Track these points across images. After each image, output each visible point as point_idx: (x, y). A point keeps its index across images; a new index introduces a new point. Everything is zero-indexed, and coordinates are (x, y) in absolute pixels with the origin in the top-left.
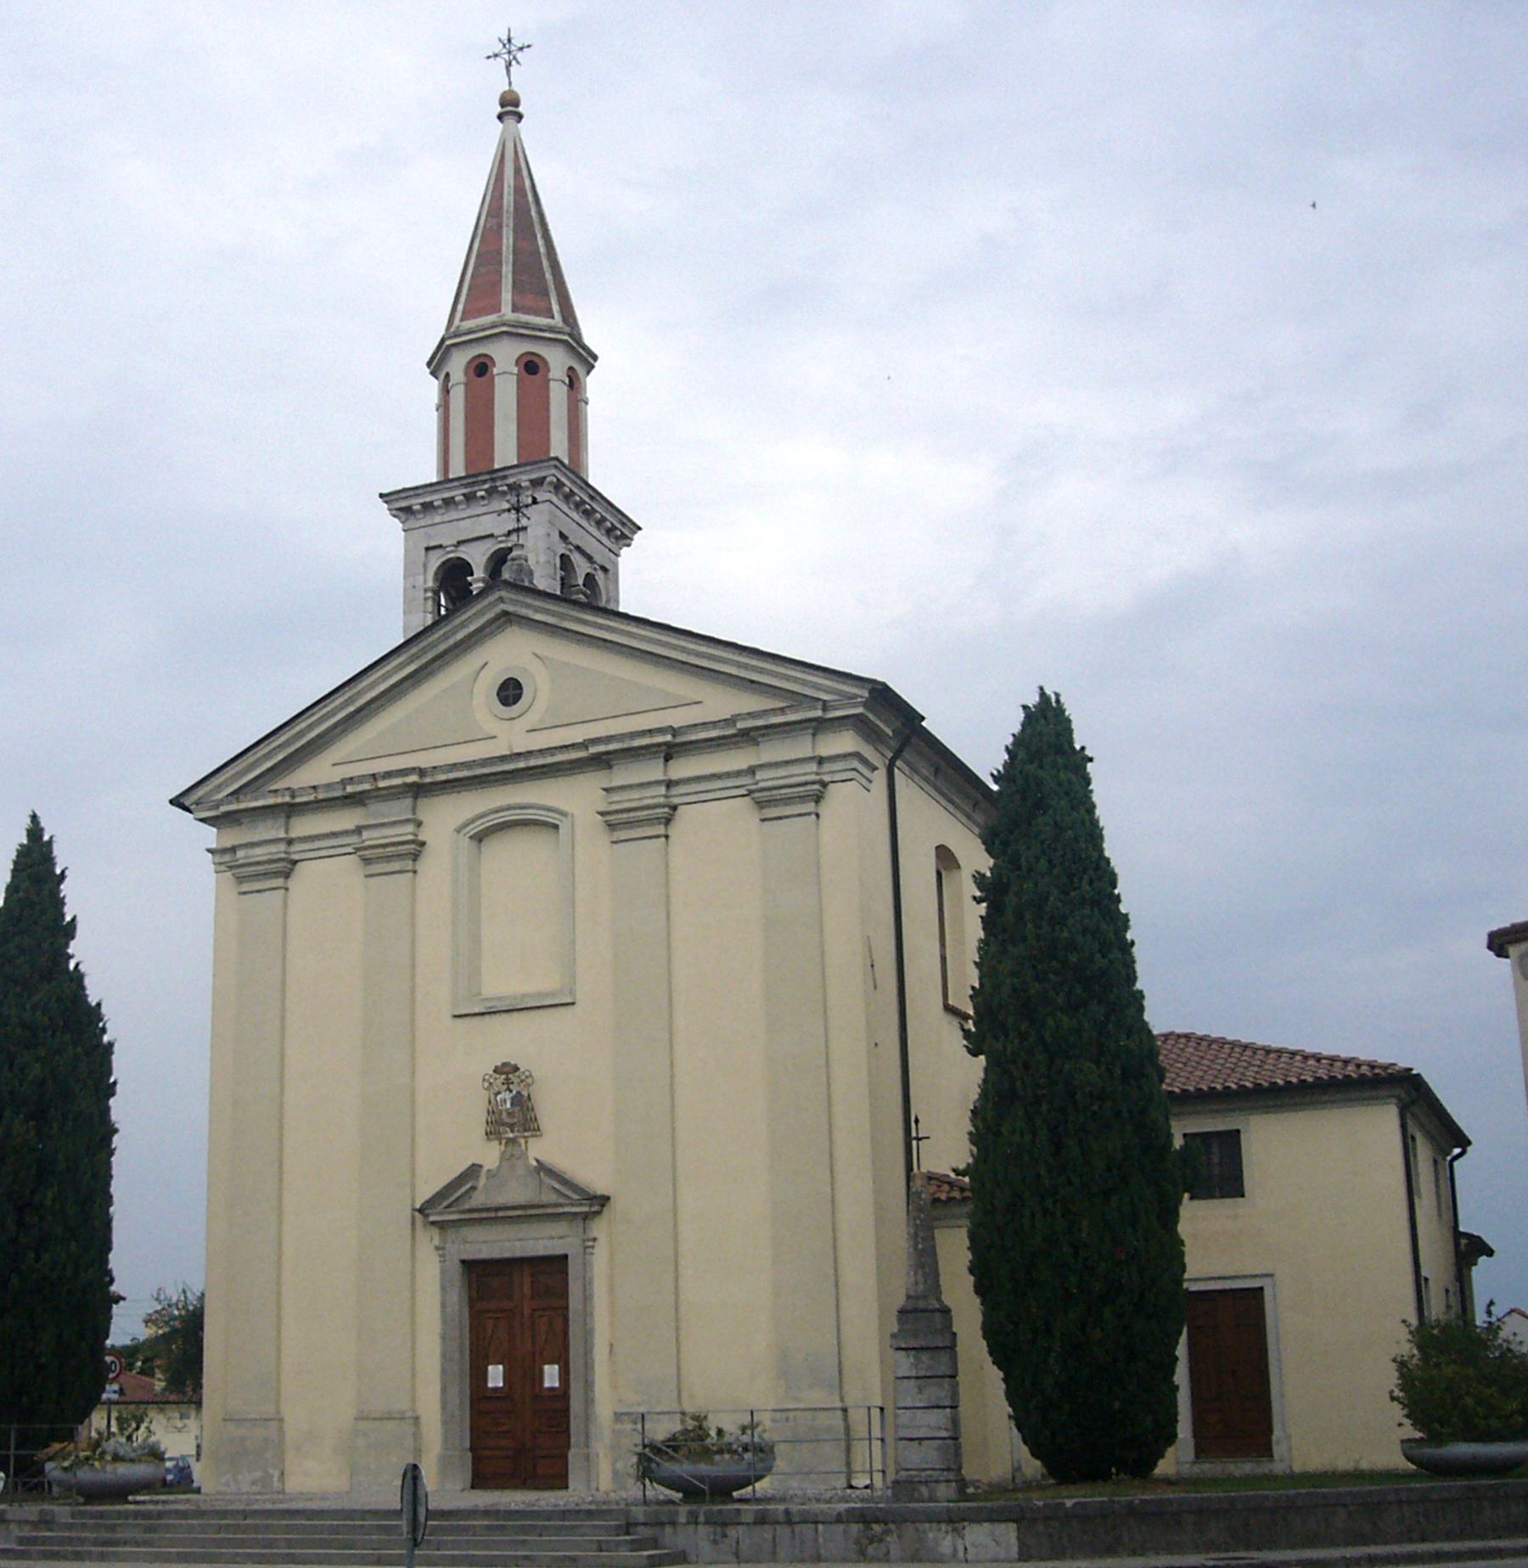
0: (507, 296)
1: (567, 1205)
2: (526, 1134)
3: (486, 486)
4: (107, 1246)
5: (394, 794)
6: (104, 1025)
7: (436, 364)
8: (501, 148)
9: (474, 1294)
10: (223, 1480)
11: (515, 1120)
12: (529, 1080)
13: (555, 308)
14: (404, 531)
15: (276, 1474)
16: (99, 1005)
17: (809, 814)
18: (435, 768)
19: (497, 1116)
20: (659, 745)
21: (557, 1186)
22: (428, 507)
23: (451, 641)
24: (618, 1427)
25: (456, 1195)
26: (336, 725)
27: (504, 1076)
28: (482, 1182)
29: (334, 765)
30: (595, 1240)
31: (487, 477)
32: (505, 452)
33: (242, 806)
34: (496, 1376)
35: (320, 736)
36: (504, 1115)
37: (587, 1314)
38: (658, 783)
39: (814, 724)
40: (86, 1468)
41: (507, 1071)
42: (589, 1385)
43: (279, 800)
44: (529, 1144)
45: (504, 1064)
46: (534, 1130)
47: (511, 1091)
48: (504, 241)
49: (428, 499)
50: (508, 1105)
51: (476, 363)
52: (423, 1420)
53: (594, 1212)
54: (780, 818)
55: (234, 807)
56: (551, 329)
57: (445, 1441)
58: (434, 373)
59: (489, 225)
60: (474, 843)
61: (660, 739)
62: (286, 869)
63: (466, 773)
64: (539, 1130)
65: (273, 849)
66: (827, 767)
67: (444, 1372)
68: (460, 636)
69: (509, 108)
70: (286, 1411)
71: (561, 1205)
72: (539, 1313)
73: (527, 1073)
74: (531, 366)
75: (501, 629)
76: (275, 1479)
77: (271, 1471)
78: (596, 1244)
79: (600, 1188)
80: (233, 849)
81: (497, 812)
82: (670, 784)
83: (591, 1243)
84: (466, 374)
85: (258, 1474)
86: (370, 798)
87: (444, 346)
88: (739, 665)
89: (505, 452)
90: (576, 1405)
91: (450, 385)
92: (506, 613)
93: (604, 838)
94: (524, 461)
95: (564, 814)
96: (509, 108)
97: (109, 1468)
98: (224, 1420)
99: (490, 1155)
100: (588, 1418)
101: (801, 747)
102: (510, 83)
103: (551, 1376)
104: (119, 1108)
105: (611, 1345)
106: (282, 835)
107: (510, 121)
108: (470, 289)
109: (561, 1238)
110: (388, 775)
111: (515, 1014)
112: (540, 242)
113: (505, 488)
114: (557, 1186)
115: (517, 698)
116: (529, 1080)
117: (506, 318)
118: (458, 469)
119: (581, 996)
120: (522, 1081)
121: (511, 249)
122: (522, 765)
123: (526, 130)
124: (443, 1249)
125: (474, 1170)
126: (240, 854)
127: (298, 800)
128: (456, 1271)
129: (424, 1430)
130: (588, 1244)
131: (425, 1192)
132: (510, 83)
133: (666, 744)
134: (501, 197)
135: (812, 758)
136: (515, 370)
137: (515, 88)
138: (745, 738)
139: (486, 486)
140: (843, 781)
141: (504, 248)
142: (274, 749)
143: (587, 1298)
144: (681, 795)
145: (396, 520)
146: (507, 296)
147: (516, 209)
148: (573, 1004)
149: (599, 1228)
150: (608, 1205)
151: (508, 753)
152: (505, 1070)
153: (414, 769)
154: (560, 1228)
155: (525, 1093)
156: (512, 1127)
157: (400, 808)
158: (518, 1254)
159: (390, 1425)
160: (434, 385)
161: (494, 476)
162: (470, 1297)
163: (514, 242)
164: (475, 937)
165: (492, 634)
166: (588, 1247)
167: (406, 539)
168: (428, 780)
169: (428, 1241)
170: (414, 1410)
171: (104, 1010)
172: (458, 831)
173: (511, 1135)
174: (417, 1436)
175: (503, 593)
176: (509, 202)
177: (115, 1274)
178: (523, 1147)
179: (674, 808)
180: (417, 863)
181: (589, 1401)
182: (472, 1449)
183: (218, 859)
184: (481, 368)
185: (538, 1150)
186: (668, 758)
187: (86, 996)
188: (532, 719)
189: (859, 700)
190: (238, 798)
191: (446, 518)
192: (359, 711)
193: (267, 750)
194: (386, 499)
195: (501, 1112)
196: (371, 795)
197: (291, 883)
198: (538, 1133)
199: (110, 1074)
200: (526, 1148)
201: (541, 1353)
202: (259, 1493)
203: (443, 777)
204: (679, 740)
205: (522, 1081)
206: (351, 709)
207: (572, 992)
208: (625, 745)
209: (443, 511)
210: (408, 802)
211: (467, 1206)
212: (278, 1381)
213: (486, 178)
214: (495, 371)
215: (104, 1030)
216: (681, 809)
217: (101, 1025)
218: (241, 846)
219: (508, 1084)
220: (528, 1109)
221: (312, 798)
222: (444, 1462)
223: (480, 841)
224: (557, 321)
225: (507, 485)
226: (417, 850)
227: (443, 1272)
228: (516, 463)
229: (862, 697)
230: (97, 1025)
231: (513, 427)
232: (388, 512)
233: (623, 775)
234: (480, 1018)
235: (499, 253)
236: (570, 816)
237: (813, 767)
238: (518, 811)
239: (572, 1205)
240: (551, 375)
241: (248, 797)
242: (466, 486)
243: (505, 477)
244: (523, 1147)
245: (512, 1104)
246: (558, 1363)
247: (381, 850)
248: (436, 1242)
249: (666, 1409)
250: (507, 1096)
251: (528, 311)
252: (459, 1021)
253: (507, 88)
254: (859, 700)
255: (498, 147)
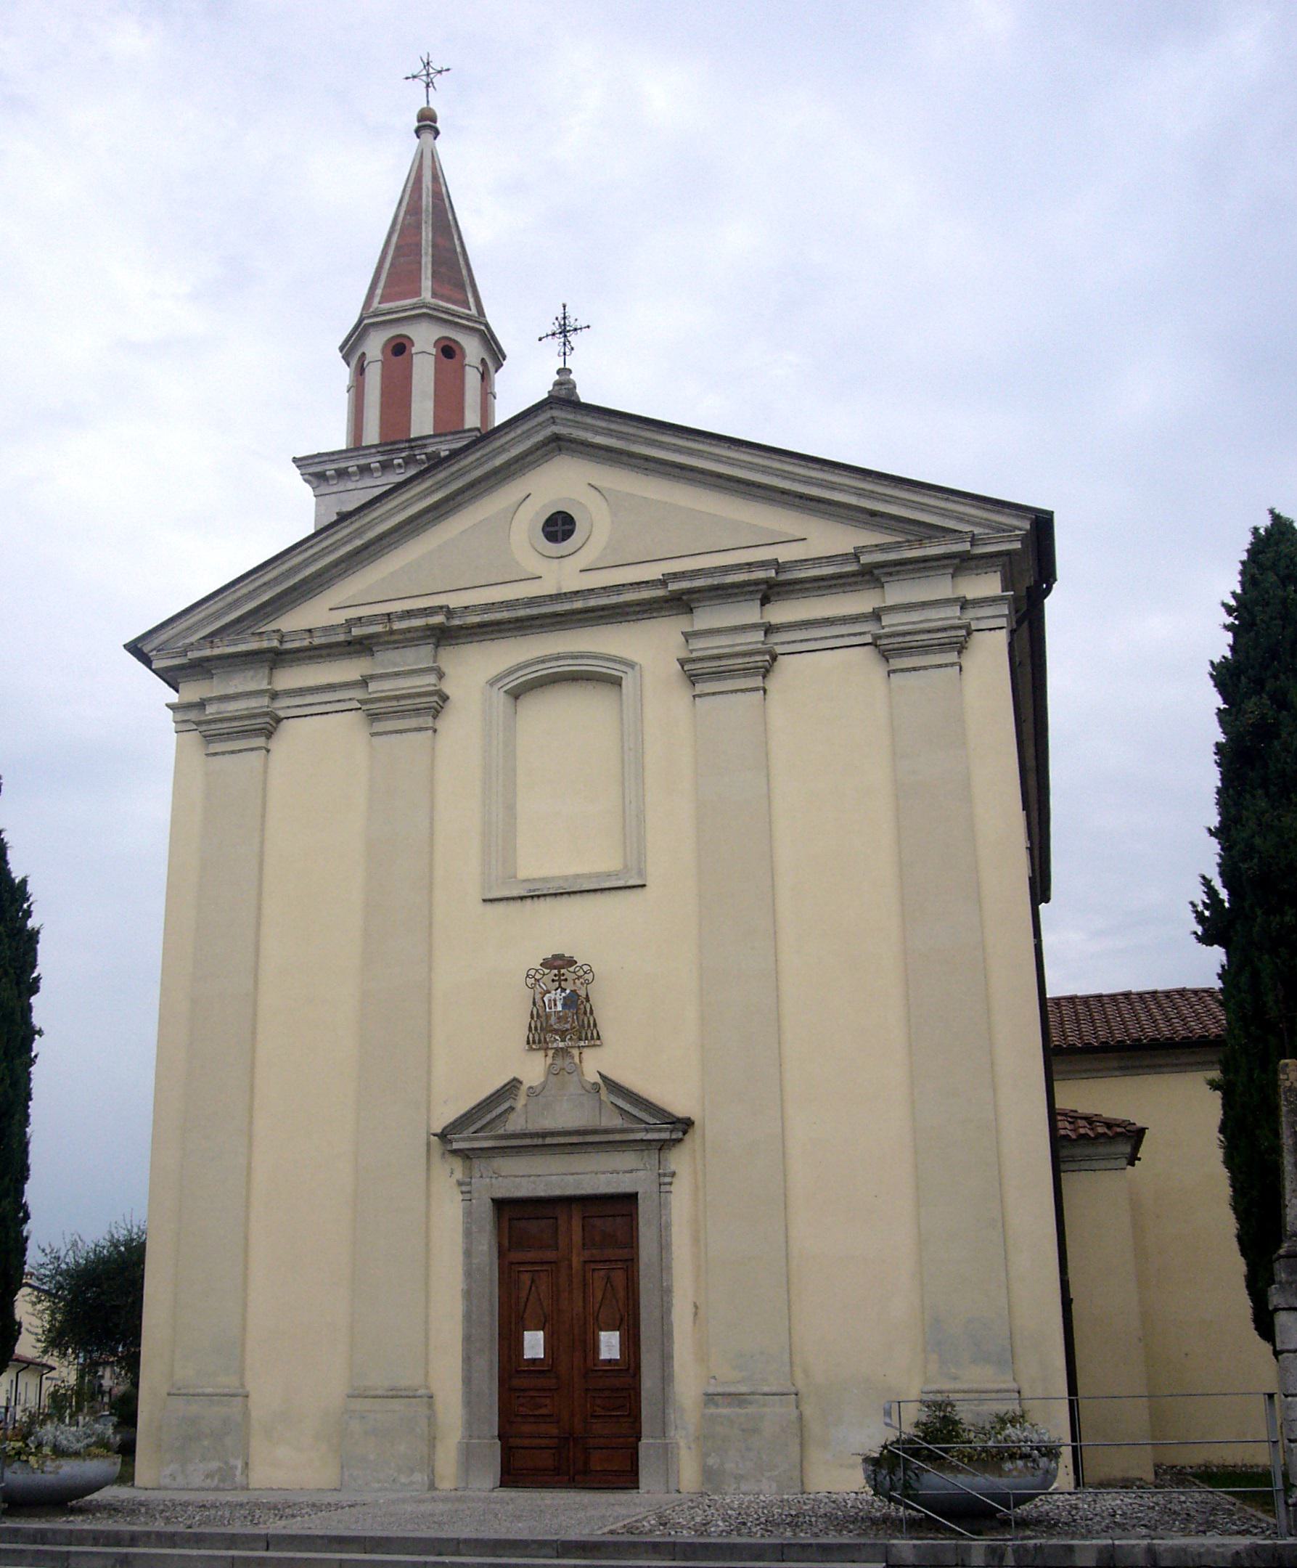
0: (427, 284)
1: (639, 1130)
2: (582, 1043)
3: (403, 455)
4: (21, 1173)
5: (413, 639)
6: (29, 906)
7: (350, 348)
8: (419, 156)
9: (506, 1243)
10: (168, 1472)
11: (568, 1026)
12: (589, 977)
13: (471, 300)
14: (315, 496)
15: (239, 1464)
16: (24, 882)
17: (952, 665)
18: (466, 608)
19: (543, 1019)
20: (756, 583)
21: (627, 1107)
22: (342, 474)
23: (487, 467)
24: (712, 1410)
25: (494, 1114)
26: (335, 564)
27: (556, 972)
28: (521, 1101)
29: (331, 609)
30: (673, 1174)
31: (407, 445)
32: (422, 421)
33: (217, 652)
34: (534, 1344)
35: (319, 574)
36: (553, 1020)
37: (664, 1266)
38: (754, 627)
39: (957, 561)
40: (16, 1465)
41: (559, 964)
42: (666, 1358)
43: (265, 644)
44: (583, 1055)
45: (556, 957)
46: (592, 1038)
47: (564, 990)
48: (424, 234)
49: (343, 465)
50: (560, 1008)
51: (393, 344)
52: (439, 1398)
53: (674, 1140)
54: (914, 669)
55: (207, 652)
56: (468, 318)
57: (469, 1424)
58: (346, 358)
59: (406, 222)
60: (511, 700)
61: (760, 574)
62: (268, 726)
63: (506, 615)
64: (599, 1038)
65: (253, 703)
66: (971, 613)
67: (467, 1339)
68: (498, 462)
69: (428, 123)
70: (250, 1387)
71: (632, 1131)
72: (593, 1266)
73: (585, 968)
74: (448, 351)
75: (547, 457)
76: (238, 1472)
77: (232, 1461)
78: (675, 1180)
79: (680, 1109)
80: (202, 705)
81: (543, 662)
82: (769, 629)
83: (667, 1180)
84: (383, 352)
85: (215, 1465)
86: (381, 644)
87: (363, 325)
88: (860, 493)
89: (422, 421)
90: (648, 1382)
91: (366, 363)
92: (556, 438)
93: (680, 697)
94: (439, 432)
95: (631, 665)
96: (428, 123)
97: (50, 1466)
98: (169, 1394)
99: (533, 1070)
100: (665, 1399)
101: (941, 587)
102: (428, 102)
103: (609, 1345)
104: (42, 1009)
105: (696, 1307)
106: (264, 686)
107: (427, 136)
108: (389, 275)
109: (631, 1171)
110: (409, 614)
111: (565, 899)
112: (457, 242)
113: (423, 457)
114: (627, 1107)
115: (568, 534)
116: (589, 977)
117: (427, 301)
118: (372, 435)
119: (654, 877)
120: (579, 978)
121: (430, 244)
122: (579, 605)
123: (441, 145)
124: (470, 1184)
125: (514, 1084)
126: (211, 709)
127: (288, 646)
128: (485, 1212)
129: (439, 1407)
130: (665, 1180)
131: (445, 1115)
132: (428, 102)
133: (766, 581)
134: (420, 197)
135: (956, 600)
136: (434, 351)
137: (431, 106)
138: (867, 577)
139: (403, 455)
140: (990, 629)
141: (423, 242)
142: (260, 587)
143: (664, 1246)
144: (783, 643)
145: (307, 485)
146: (427, 284)
147: (434, 207)
148: (644, 886)
149: (679, 1160)
150: (691, 1131)
151: (554, 592)
152: (560, 962)
153: (441, 607)
154: (627, 1160)
155: (582, 993)
156: (563, 1034)
157: (419, 656)
158: (570, 1191)
159: (396, 1405)
160: (344, 374)
161: (413, 444)
162: (500, 1246)
163: (433, 237)
164: (511, 808)
165: (536, 464)
166: (665, 1184)
167: (317, 505)
168: (456, 622)
169: (448, 1175)
170: (428, 1388)
171: (30, 889)
172: (492, 683)
173: (561, 1045)
174: (431, 1419)
175: (556, 413)
176: (428, 202)
177: (31, 1209)
178: (577, 1060)
179: (774, 658)
180: (437, 720)
181: (666, 1378)
182: (500, 1437)
183: (180, 717)
184: (399, 348)
185: (593, 1064)
186: (765, 601)
187: (9, 873)
188: (583, 559)
189: (1018, 532)
190: (212, 642)
191: (360, 485)
192: (366, 547)
193: (251, 587)
194: (299, 463)
195: (548, 1016)
196: (381, 640)
197: (275, 744)
198: (598, 1042)
199: (34, 966)
200: (581, 1062)
201: (596, 1319)
202: (217, 1489)
203: (477, 619)
204: (782, 577)
205: (579, 978)
206: (358, 543)
207: (641, 873)
208: (716, 581)
209: (357, 478)
210: (427, 650)
211: (501, 1131)
212: (243, 1345)
213: (410, 164)
214: (414, 350)
215: (28, 914)
216: (780, 657)
217: (25, 906)
218: (211, 700)
219: (560, 981)
220: (585, 1013)
221: (306, 643)
222: (468, 1455)
223: (516, 697)
224: (474, 311)
225: (425, 454)
226: (437, 704)
227: (468, 1214)
228: (432, 433)
229: (1020, 530)
230: (22, 906)
231: (430, 405)
232: (301, 477)
233: (707, 618)
234: (519, 904)
235: (419, 245)
236: (637, 668)
237: (955, 611)
238: (571, 662)
239: (647, 1131)
240: (467, 361)
241: (226, 643)
242: (383, 453)
243: (425, 446)
244: (577, 1060)
245: (564, 1005)
246: (618, 1330)
247: (395, 703)
248: (459, 1175)
249: (774, 1389)
250: (559, 996)
251: (442, 298)
252: (489, 906)
253: (425, 105)
254: (1018, 532)
255: (416, 154)
